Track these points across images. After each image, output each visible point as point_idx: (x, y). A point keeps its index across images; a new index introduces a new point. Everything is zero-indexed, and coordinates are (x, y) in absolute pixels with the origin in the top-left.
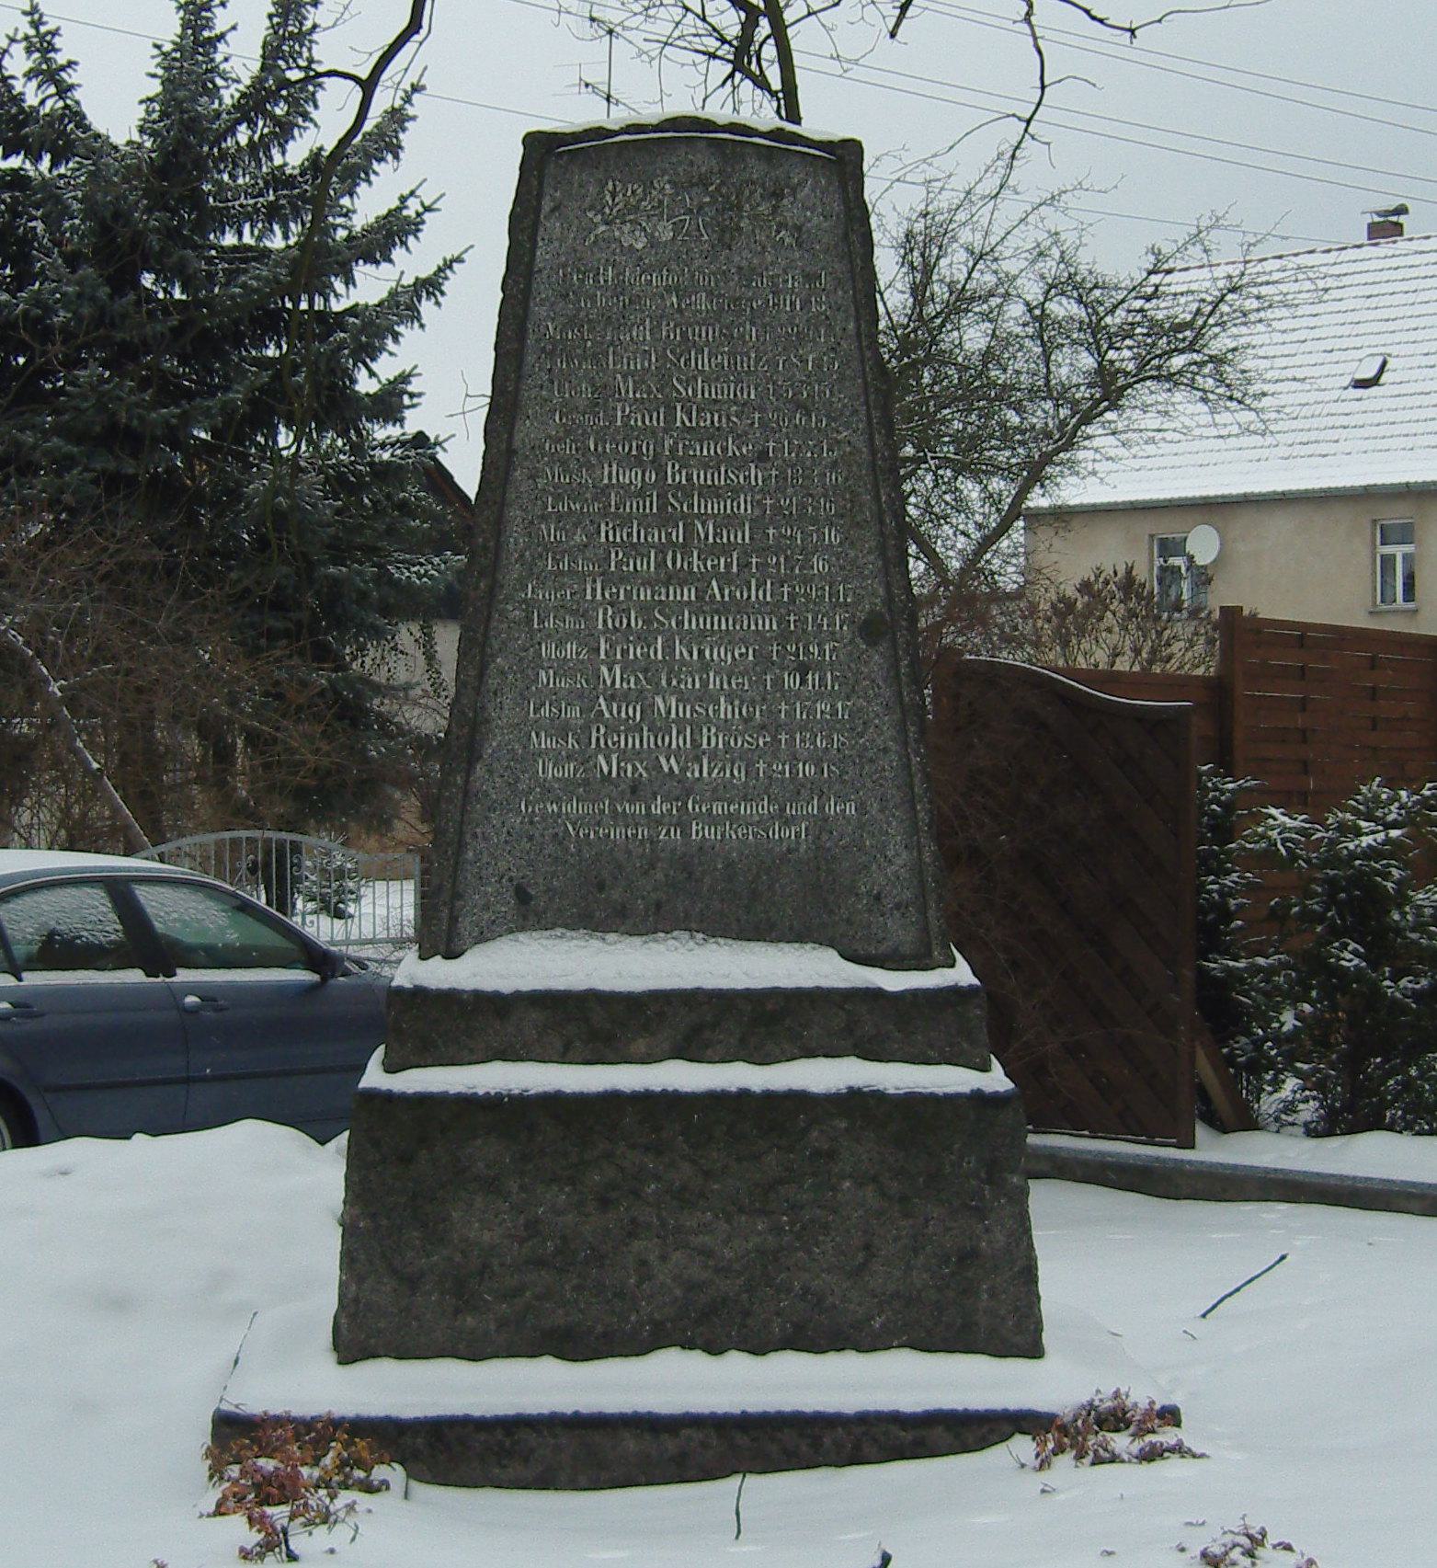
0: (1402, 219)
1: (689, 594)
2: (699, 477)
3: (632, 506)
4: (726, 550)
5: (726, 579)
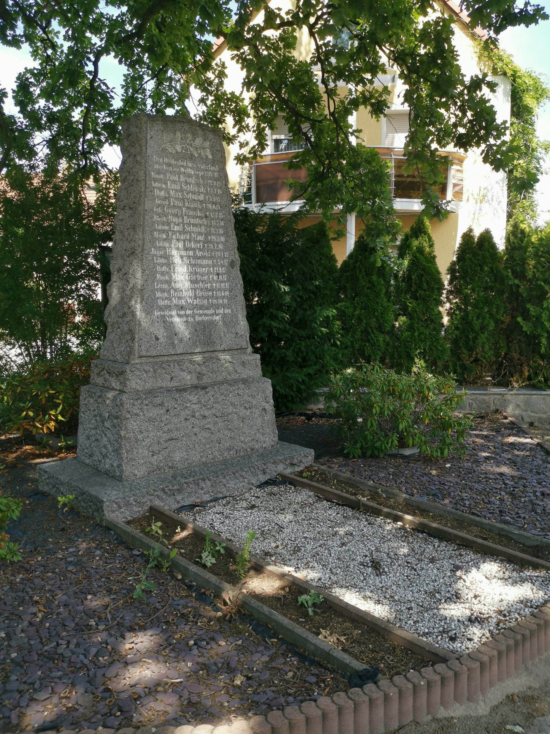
1: (191, 253)
2: (192, 221)
3: (176, 228)
5: (200, 250)
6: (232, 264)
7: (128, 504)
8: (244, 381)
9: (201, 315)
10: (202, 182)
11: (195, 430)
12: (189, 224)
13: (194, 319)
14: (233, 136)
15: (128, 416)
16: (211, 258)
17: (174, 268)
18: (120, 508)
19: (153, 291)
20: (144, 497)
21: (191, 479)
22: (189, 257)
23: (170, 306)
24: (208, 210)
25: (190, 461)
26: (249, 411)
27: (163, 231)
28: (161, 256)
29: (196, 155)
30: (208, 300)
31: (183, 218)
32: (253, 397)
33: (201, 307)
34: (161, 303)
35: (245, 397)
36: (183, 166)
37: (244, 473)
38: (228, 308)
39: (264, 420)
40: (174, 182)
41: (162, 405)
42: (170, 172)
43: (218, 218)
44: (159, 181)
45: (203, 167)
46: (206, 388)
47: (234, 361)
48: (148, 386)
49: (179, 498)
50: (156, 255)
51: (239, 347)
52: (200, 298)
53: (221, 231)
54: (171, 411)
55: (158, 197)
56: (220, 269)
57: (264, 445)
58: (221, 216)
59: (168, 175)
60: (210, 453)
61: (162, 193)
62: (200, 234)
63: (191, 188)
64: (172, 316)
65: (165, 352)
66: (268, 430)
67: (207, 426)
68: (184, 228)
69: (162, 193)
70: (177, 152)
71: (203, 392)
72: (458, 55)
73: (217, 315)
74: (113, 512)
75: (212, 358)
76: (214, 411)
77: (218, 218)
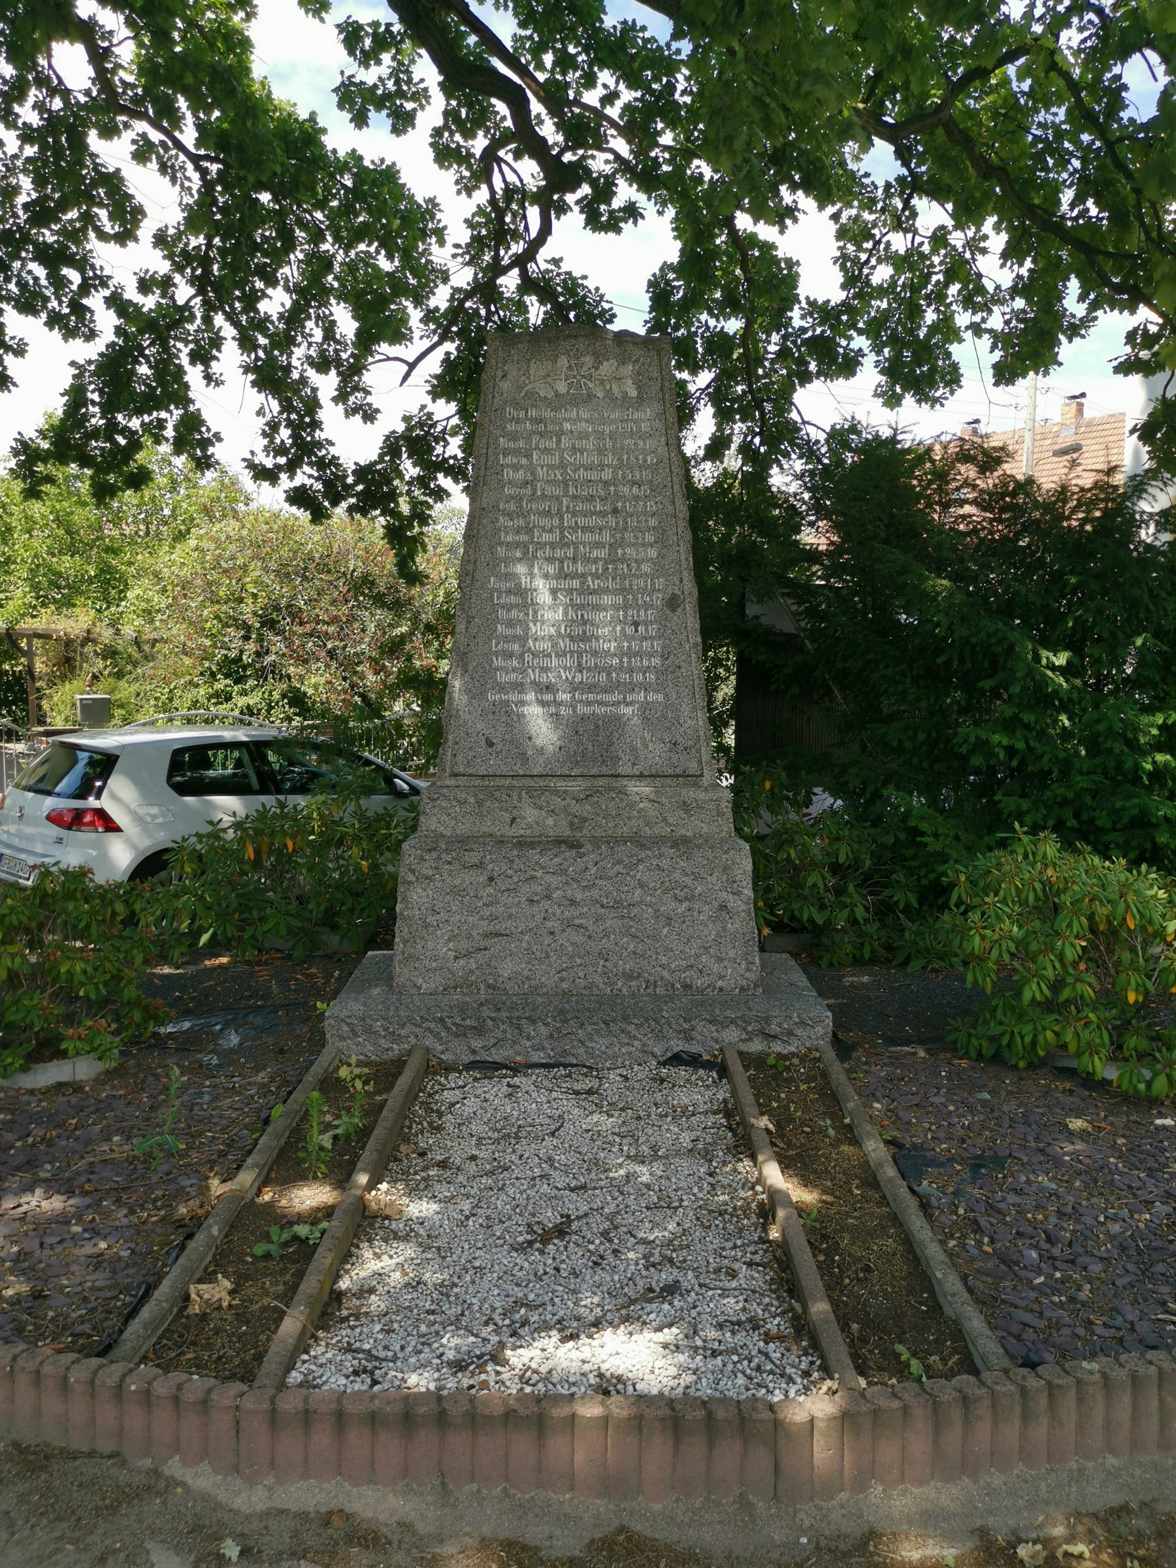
0: (1083, 400)
1: (576, 584)
2: (582, 521)
3: (546, 537)
4: (596, 561)
5: (596, 576)
6: (673, 603)
7: (370, 1032)
8: (682, 844)
9: (589, 703)
10: (609, 444)
11: (549, 924)
12: (575, 528)
13: (574, 711)
14: (1081, 319)
15: (411, 878)
16: (622, 591)
17: (536, 612)
18: (356, 1035)
19: (488, 655)
20: (403, 1026)
21: (504, 1014)
22: (570, 591)
23: (522, 684)
24: (619, 496)
25: (534, 983)
26: (686, 904)
27: (517, 545)
28: (509, 592)
29: (600, 395)
30: (609, 674)
31: (562, 518)
32: (697, 877)
33: (591, 688)
34: (502, 678)
35: (677, 875)
36: (568, 420)
37: (631, 1028)
38: (655, 691)
39: (724, 929)
40: (547, 451)
41: (480, 865)
42: (541, 434)
43: (645, 513)
44: (516, 452)
45: (615, 415)
46: (581, 846)
47: (663, 800)
48: (464, 828)
49: (477, 1044)
50: (497, 590)
51: (678, 771)
52: (589, 669)
53: (649, 538)
54: (499, 882)
55: (510, 482)
56: (642, 613)
57: (720, 983)
58: (651, 506)
59: (535, 439)
60: (581, 974)
61: (520, 475)
62: (599, 545)
63: (585, 459)
64: (523, 703)
65: (505, 770)
66: (732, 953)
67: (577, 922)
68: (563, 537)
69: (520, 475)
70: (557, 395)
71: (574, 852)
72: (382, 160)
73: (631, 704)
74: (343, 1039)
75: (611, 789)
76: (595, 893)
77: (645, 513)
